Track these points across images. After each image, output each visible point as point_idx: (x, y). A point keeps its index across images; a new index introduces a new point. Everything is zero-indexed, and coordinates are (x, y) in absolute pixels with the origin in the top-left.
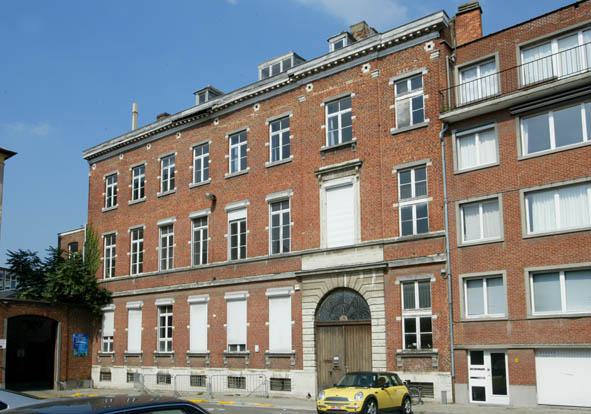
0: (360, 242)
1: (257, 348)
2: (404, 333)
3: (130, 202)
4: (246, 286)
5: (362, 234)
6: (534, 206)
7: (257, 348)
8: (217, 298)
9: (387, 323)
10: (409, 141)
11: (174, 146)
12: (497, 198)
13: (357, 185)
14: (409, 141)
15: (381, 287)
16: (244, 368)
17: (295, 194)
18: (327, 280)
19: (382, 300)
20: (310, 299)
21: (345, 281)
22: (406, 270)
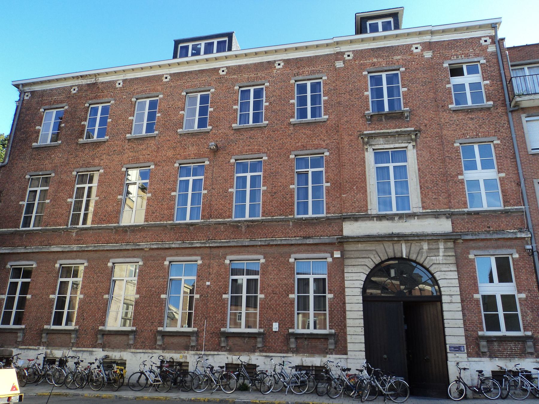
0: (421, 210)
1: (275, 326)
2: (483, 313)
3: (81, 141)
4: (262, 250)
5: (423, 202)
6: (373, 263)
7: (275, 326)
8: (214, 263)
9: (462, 301)
10: (472, 119)
11: (159, 88)
12: (410, 210)
13: (529, 149)
14: (472, 119)
15: (452, 260)
16: (254, 351)
17: (331, 154)
18: (379, 247)
19: (455, 275)
20: (355, 269)
21: (404, 250)
22: (481, 244)
